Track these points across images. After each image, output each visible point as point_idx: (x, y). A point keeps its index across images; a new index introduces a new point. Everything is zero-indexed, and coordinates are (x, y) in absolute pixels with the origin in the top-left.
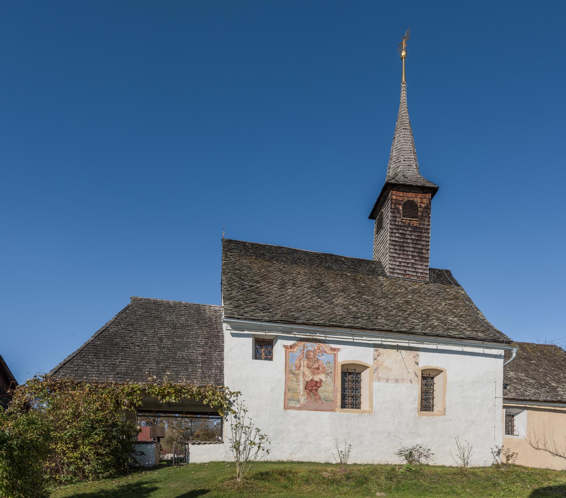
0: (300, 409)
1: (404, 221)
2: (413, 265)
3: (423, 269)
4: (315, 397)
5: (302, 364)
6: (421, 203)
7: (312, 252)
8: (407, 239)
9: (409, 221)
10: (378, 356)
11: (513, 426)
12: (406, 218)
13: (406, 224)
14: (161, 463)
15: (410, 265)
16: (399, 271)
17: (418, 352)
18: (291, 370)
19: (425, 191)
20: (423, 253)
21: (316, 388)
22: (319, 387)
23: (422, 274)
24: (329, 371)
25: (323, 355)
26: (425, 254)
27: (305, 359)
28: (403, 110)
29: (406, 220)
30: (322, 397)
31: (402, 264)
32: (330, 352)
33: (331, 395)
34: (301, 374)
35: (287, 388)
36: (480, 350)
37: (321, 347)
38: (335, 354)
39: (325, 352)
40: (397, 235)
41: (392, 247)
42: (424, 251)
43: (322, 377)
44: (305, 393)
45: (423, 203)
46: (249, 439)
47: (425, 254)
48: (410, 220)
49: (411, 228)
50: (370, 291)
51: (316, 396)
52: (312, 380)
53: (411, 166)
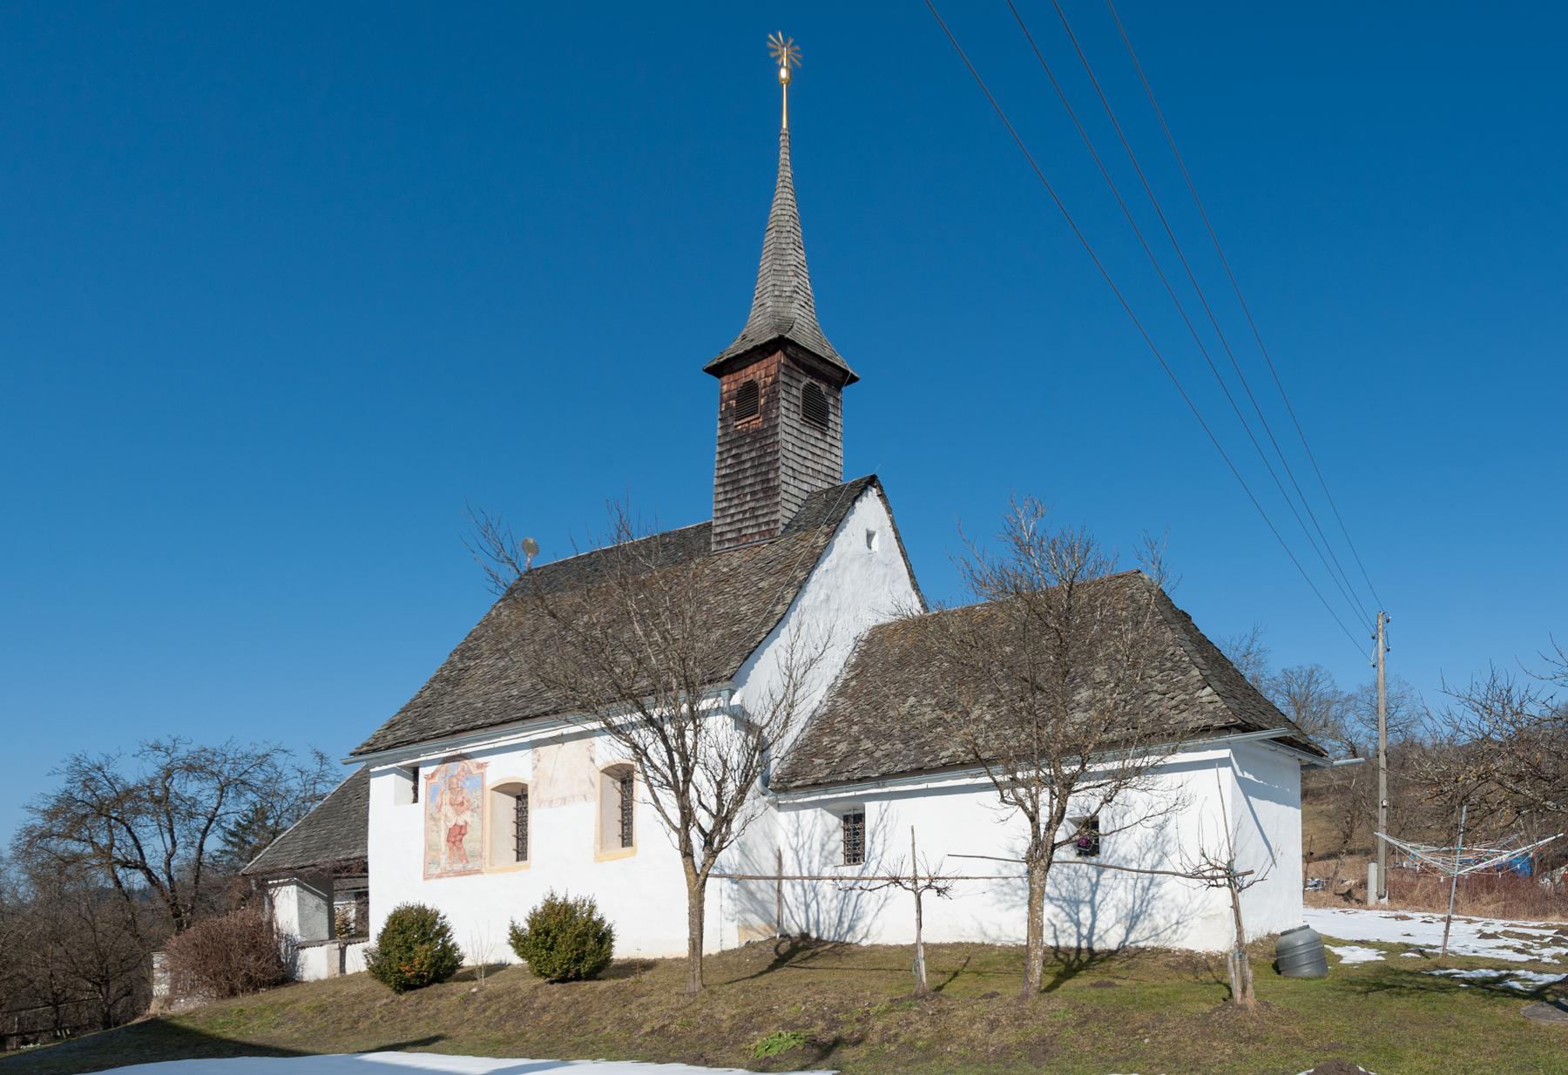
0: (440, 876)
1: (739, 427)
6: (766, 377)
9: (747, 425)
11: (345, 969)
14: (129, 1024)
15: (748, 515)
17: (592, 740)
20: (768, 480)
22: (464, 835)
23: (769, 525)
24: (476, 805)
28: (784, 203)
29: (742, 424)
33: (478, 846)
34: (443, 818)
38: (482, 773)
40: (729, 461)
43: (467, 817)
44: (448, 848)
47: (774, 479)
52: (455, 825)
53: (763, 304)
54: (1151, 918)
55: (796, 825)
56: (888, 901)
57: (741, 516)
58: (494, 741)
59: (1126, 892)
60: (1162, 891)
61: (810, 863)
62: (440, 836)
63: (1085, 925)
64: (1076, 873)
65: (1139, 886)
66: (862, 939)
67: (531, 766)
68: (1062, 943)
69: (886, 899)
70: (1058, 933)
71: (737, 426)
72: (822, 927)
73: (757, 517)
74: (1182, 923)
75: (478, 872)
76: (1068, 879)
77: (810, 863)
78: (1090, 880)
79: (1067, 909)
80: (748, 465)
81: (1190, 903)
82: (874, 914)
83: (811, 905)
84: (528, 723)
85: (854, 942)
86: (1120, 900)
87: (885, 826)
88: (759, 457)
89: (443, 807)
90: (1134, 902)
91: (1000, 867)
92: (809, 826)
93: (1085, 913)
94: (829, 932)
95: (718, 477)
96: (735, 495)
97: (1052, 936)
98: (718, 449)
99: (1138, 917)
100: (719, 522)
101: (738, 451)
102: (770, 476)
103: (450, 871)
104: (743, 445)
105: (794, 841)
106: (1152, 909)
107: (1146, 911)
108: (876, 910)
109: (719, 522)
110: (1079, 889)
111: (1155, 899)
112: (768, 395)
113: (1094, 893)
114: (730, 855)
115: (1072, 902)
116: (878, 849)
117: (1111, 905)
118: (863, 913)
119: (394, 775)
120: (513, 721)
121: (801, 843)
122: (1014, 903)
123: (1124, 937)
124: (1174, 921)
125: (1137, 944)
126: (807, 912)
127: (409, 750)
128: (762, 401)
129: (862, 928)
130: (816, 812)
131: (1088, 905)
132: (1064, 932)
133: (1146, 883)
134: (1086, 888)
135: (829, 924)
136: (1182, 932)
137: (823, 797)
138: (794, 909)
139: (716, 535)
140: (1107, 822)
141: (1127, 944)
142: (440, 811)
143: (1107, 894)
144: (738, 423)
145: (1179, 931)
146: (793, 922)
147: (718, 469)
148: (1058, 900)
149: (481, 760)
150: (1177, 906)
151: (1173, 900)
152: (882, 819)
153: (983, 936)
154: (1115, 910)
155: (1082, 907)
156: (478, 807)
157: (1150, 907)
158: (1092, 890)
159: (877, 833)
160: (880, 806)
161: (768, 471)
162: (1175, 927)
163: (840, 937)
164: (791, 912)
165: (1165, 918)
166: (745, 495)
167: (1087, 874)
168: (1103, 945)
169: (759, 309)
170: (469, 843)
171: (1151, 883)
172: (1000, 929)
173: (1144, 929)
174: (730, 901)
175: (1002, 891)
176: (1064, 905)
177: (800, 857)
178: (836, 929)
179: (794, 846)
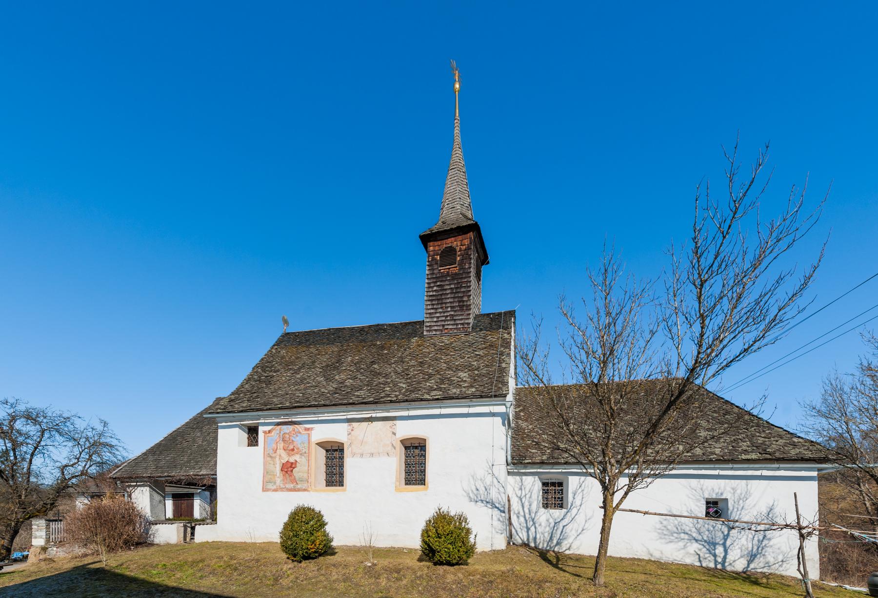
1: (442, 271)
2: (453, 318)
3: (464, 319)
4: (290, 478)
5: (279, 447)
6: (461, 245)
7: (358, 327)
8: (446, 290)
9: (447, 270)
10: (352, 430)
12: (444, 268)
13: (444, 273)
15: (449, 318)
16: (436, 328)
17: (394, 422)
18: (269, 454)
21: (292, 469)
22: (294, 468)
24: (304, 451)
25: (297, 436)
26: (467, 301)
27: (281, 442)
29: (444, 269)
30: (297, 478)
31: (440, 319)
32: (304, 432)
33: (305, 475)
34: (278, 457)
35: (265, 472)
36: (464, 410)
37: (296, 428)
39: (300, 433)
40: (435, 288)
41: (429, 303)
42: (465, 299)
43: (297, 457)
44: (282, 475)
45: (463, 245)
46: (733, 532)
47: (467, 301)
49: (450, 277)
50: (418, 355)
51: (292, 477)
52: (287, 461)
53: (454, 207)
54: (765, 557)
55: (520, 484)
56: (584, 531)
57: (444, 318)
58: (319, 416)
59: (747, 541)
60: (771, 543)
61: (530, 505)
62: (276, 467)
63: (720, 557)
64: (714, 528)
65: (756, 539)
66: (566, 550)
67: (346, 433)
68: (704, 565)
69: (583, 530)
70: (701, 559)
71: (441, 270)
72: (538, 541)
73: (455, 320)
74: (785, 561)
75: (305, 490)
76: (708, 531)
77: (530, 505)
78: (723, 532)
79: (707, 547)
80: (448, 292)
81: (790, 551)
82: (574, 537)
83: (531, 529)
84: (350, 407)
85: (560, 551)
86: (743, 545)
87: (583, 491)
88: (457, 288)
90: (753, 547)
91: (662, 520)
92: (530, 485)
93: (720, 550)
94: (543, 544)
95: (427, 296)
96: (440, 307)
97: (698, 560)
98: (427, 281)
99: (755, 556)
100: (428, 320)
101: (442, 284)
102: (464, 299)
103: (284, 488)
104: (445, 281)
105: (519, 494)
106: (765, 552)
107: (761, 553)
108: (576, 536)
109: (428, 320)
110: (715, 537)
111: (767, 547)
112: (463, 256)
113: (726, 540)
114: (499, 497)
115: (711, 543)
116: (578, 502)
117: (737, 547)
118: (567, 536)
119: (238, 428)
120: (341, 405)
121: (524, 494)
122: (671, 540)
123: (746, 565)
124: (780, 560)
125: (756, 570)
126: (528, 532)
127: (258, 414)
128: (458, 258)
129: (566, 544)
130: (535, 478)
131: (722, 546)
132: (706, 559)
133: (761, 538)
134: (720, 536)
135: (544, 540)
136: (785, 567)
137: (539, 470)
138: (519, 530)
139: (427, 326)
140: (735, 502)
141: (749, 569)
142: (275, 453)
143: (734, 541)
144: (442, 268)
145: (784, 566)
146: (518, 537)
147: (427, 292)
148: (701, 541)
150: (782, 552)
151: (779, 549)
152: (580, 486)
153: (650, 556)
154: (739, 551)
155: (717, 546)
156: (305, 453)
157: (764, 550)
158: (724, 538)
159: (577, 493)
160: (580, 479)
161: (463, 296)
162: (781, 563)
163: (551, 548)
164: (516, 531)
165: (774, 558)
166: (448, 307)
167: (721, 529)
168: (733, 568)
169: (451, 210)
170: (297, 472)
171: (764, 538)
172: (662, 553)
173: (760, 562)
174: (499, 522)
175: (663, 533)
176: (706, 544)
177: (523, 502)
178: (548, 543)
179: (519, 495)
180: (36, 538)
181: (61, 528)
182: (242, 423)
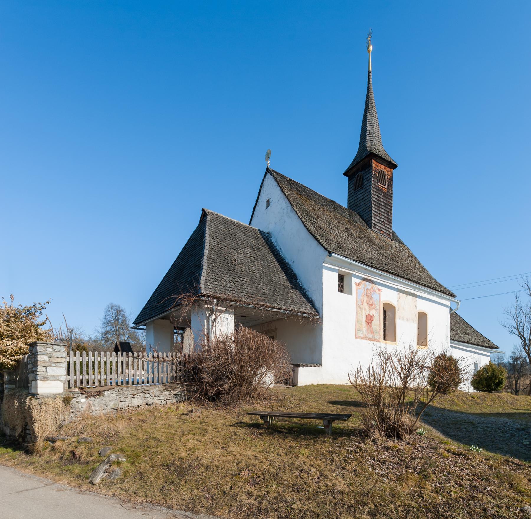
19: (390, 166)
22: (372, 321)
34: (364, 308)
48: (383, 187)
52: (369, 314)
89: (364, 303)
149: (380, 287)
180: (45, 379)
181: (158, 372)
182: (341, 269)
